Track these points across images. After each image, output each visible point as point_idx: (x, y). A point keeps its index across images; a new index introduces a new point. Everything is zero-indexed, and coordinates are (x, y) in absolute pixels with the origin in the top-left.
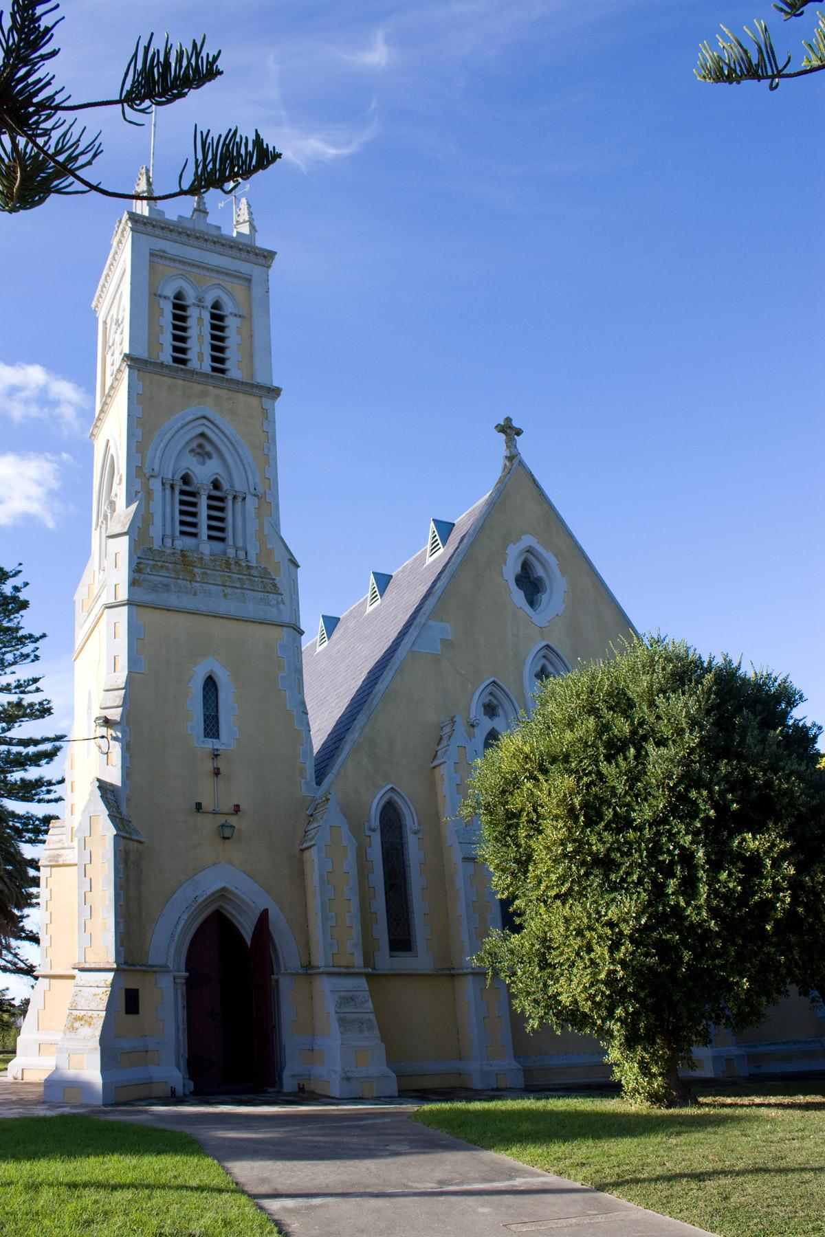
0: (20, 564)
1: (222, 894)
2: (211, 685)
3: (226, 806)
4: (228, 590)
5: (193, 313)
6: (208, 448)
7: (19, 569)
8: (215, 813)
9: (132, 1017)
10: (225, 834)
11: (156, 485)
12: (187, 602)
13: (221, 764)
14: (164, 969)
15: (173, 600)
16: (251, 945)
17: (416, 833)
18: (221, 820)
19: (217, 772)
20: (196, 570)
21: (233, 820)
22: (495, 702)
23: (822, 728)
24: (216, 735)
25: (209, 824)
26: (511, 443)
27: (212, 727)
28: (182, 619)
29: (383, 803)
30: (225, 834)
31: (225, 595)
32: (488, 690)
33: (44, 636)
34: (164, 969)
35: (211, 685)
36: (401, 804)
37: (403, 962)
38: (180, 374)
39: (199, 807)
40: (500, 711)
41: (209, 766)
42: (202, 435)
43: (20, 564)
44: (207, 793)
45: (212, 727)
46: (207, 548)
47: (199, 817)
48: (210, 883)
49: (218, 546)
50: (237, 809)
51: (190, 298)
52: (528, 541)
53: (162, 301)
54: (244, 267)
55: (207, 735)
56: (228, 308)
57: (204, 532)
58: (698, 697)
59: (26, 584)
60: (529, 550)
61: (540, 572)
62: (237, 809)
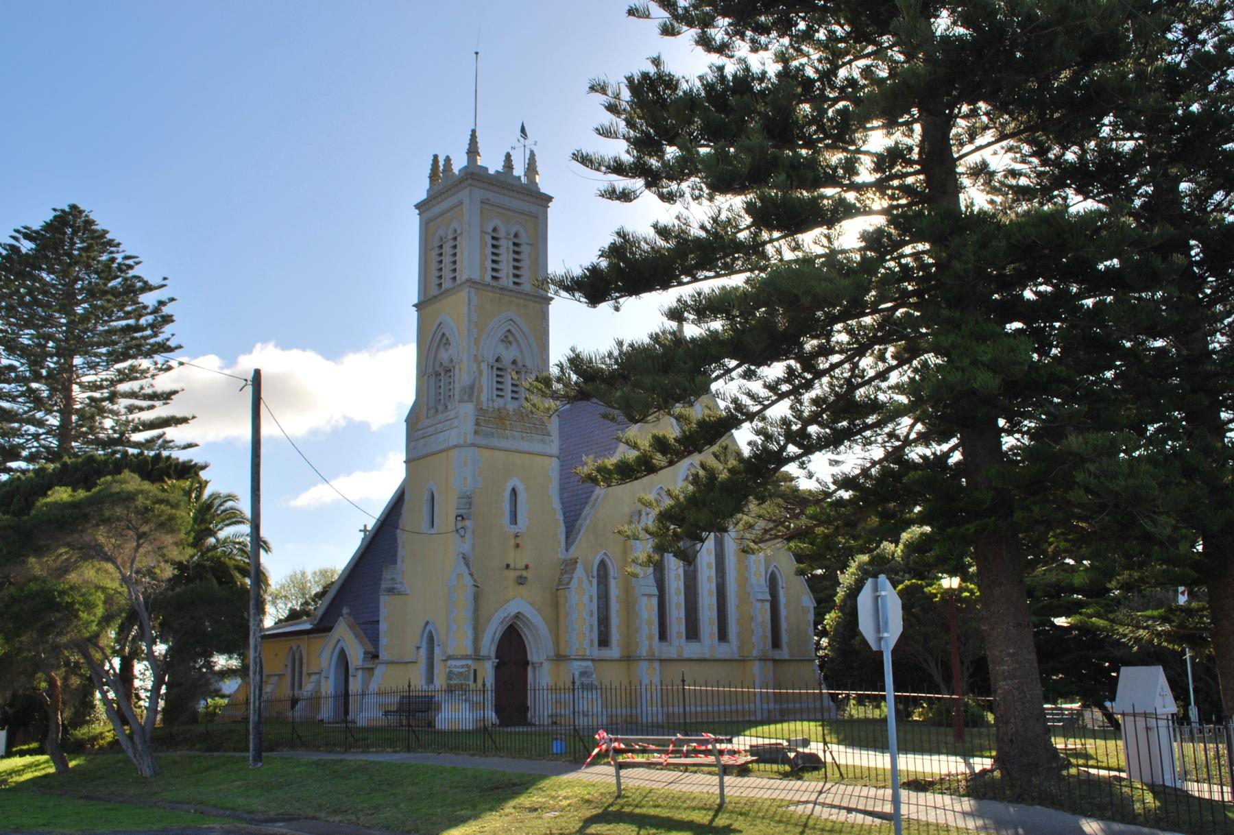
0: (165, 279)
1: (518, 616)
2: (514, 491)
3: (521, 564)
4: (524, 435)
5: (503, 243)
6: (511, 338)
7: (164, 282)
8: (515, 569)
11: (484, 366)
12: (504, 443)
14: (488, 658)
15: (495, 442)
16: (120, 669)
17: (615, 578)
18: (518, 573)
19: (517, 546)
20: (507, 422)
21: (524, 573)
25: (512, 575)
28: (501, 454)
30: (521, 581)
31: (523, 438)
33: (180, 347)
34: (488, 658)
35: (514, 491)
36: (610, 564)
39: (508, 566)
41: (512, 542)
42: (509, 331)
43: (165, 279)
44: (512, 557)
46: (511, 406)
48: (512, 608)
49: (516, 404)
51: (502, 233)
53: (486, 236)
55: (511, 524)
56: (523, 239)
57: (510, 395)
58: (859, 188)
59: (172, 300)
62: (527, 567)
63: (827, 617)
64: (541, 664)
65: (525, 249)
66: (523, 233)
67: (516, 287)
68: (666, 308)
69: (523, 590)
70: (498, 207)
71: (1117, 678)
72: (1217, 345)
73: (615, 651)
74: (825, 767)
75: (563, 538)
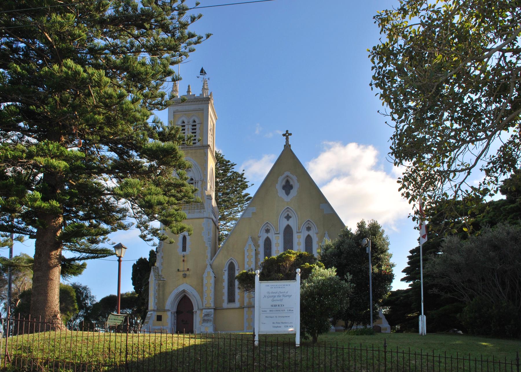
1: (184, 291)
4: (190, 211)
9: (159, 322)
10: (185, 276)
13: (185, 259)
14: (169, 310)
19: (184, 261)
21: (188, 273)
22: (269, 228)
23: (307, 228)
24: (185, 251)
25: (182, 273)
26: (287, 139)
27: (184, 249)
29: (229, 263)
30: (185, 276)
32: (307, 223)
34: (169, 310)
37: (232, 305)
38: (189, 149)
39: (178, 270)
40: (312, 228)
41: (182, 259)
45: (184, 249)
47: (179, 272)
48: (181, 289)
50: (188, 269)
52: (287, 173)
54: (201, 106)
60: (287, 176)
61: (291, 183)
62: (188, 269)
63: (38, 193)
64: (196, 311)
65: (198, 127)
66: (197, 120)
67: (195, 145)
68: (286, 196)
69: (187, 280)
70: (186, 111)
71: (265, 257)
72: (473, 193)
73: (237, 304)
74: (210, 146)
75: (209, 255)
